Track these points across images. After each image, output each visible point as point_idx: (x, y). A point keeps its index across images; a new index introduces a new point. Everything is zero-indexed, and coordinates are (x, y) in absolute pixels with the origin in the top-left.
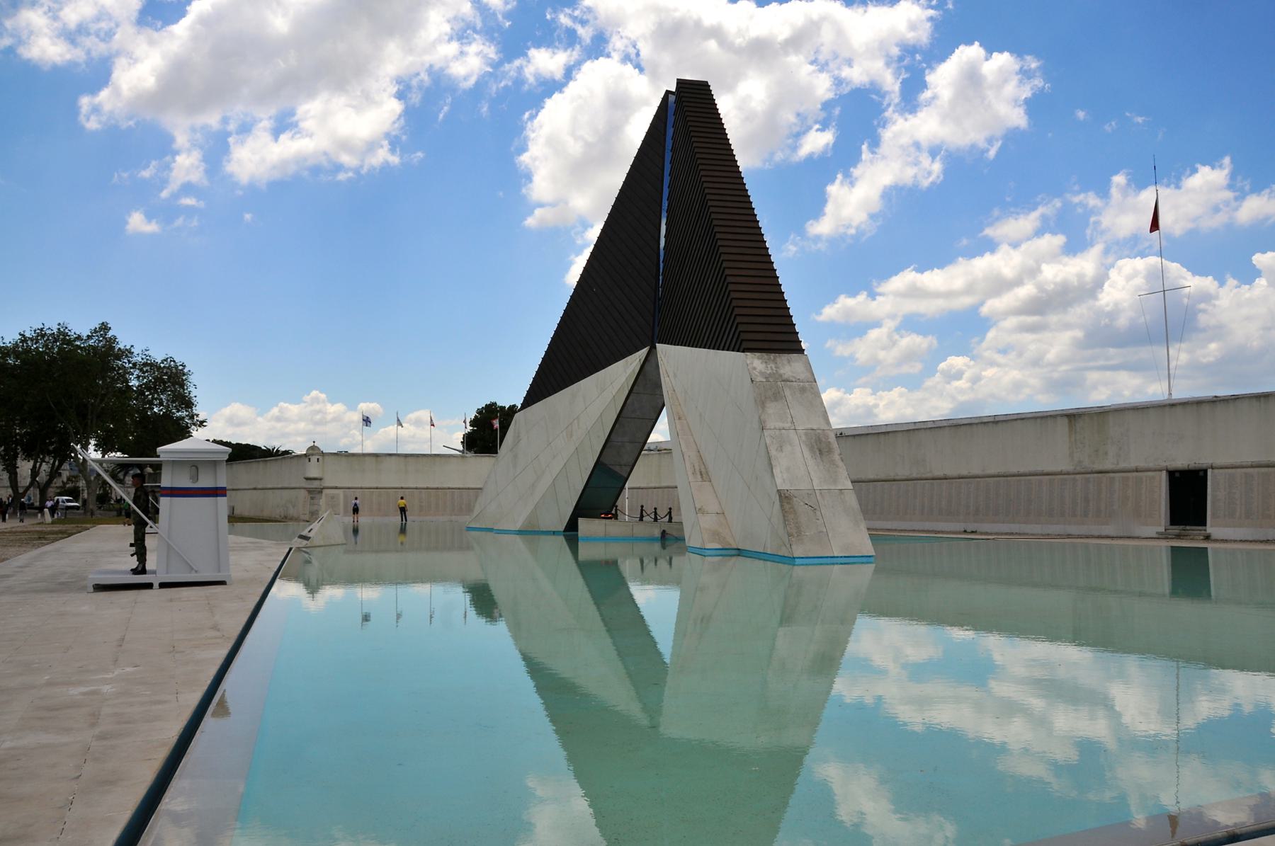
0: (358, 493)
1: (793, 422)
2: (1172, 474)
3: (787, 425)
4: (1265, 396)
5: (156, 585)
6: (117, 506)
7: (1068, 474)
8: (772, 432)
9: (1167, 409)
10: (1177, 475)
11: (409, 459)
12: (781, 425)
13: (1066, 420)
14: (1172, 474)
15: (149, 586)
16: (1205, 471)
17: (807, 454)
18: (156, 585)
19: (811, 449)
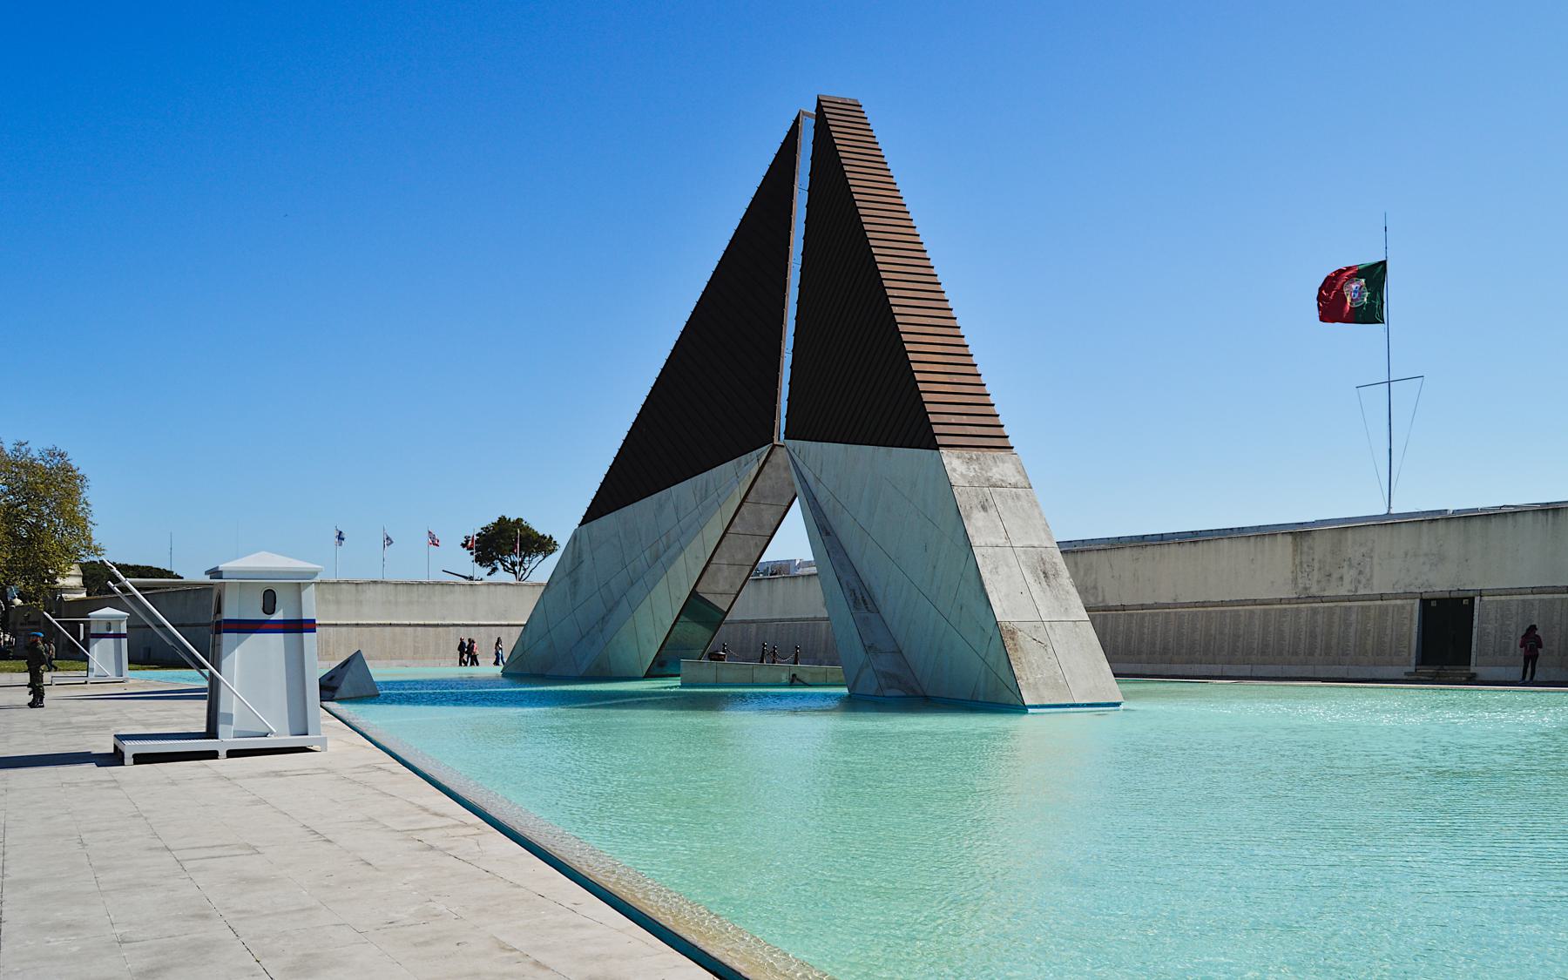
0: (473, 633)
1: (1007, 538)
2: (1425, 603)
3: (1001, 542)
4: (1551, 510)
5: (222, 753)
6: (1335, 576)
7: (1289, 601)
8: (983, 550)
9: (1425, 526)
10: (1433, 604)
11: (1520, 517)
12: (994, 541)
13: (1284, 545)
14: (1425, 603)
15: (213, 755)
16: (1472, 600)
17: (1030, 579)
18: (222, 753)
19: (1034, 571)
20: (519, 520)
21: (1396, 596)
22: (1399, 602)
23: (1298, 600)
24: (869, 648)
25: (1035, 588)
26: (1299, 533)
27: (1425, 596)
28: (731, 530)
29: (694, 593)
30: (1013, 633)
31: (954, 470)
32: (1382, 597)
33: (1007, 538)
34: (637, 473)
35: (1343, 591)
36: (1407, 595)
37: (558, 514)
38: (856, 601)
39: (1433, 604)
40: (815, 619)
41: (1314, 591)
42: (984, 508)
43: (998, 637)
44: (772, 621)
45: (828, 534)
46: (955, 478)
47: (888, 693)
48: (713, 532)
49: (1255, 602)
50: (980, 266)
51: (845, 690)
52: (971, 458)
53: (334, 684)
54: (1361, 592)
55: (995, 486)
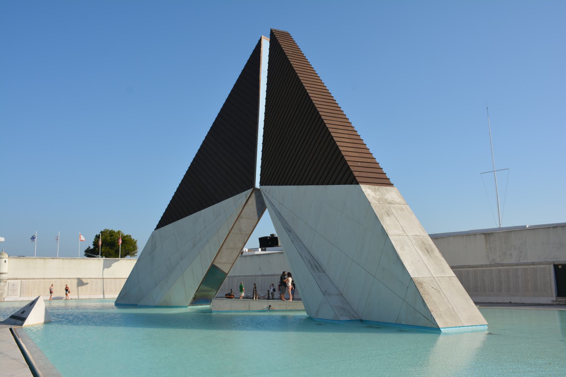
1: (404, 231)
7: (486, 266)
10: (560, 267)
17: (421, 253)
20: (119, 232)
21: (541, 263)
22: (542, 266)
23: (491, 265)
24: (325, 293)
25: (424, 258)
26: (487, 234)
27: (556, 263)
28: (232, 231)
29: (212, 263)
30: (421, 284)
31: (369, 195)
32: (533, 264)
33: (404, 231)
34: (194, 195)
35: (513, 261)
36: (549, 263)
37: (141, 225)
38: (312, 267)
39: (560, 267)
40: (256, 276)
41: (498, 261)
42: (388, 215)
43: (410, 286)
44: (235, 277)
45: (290, 232)
46: (370, 199)
47: (342, 318)
48: (224, 232)
49: (469, 267)
50: (358, 99)
51: (304, 314)
52: (375, 189)
53: (23, 316)
54: (522, 261)
55: (390, 203)
